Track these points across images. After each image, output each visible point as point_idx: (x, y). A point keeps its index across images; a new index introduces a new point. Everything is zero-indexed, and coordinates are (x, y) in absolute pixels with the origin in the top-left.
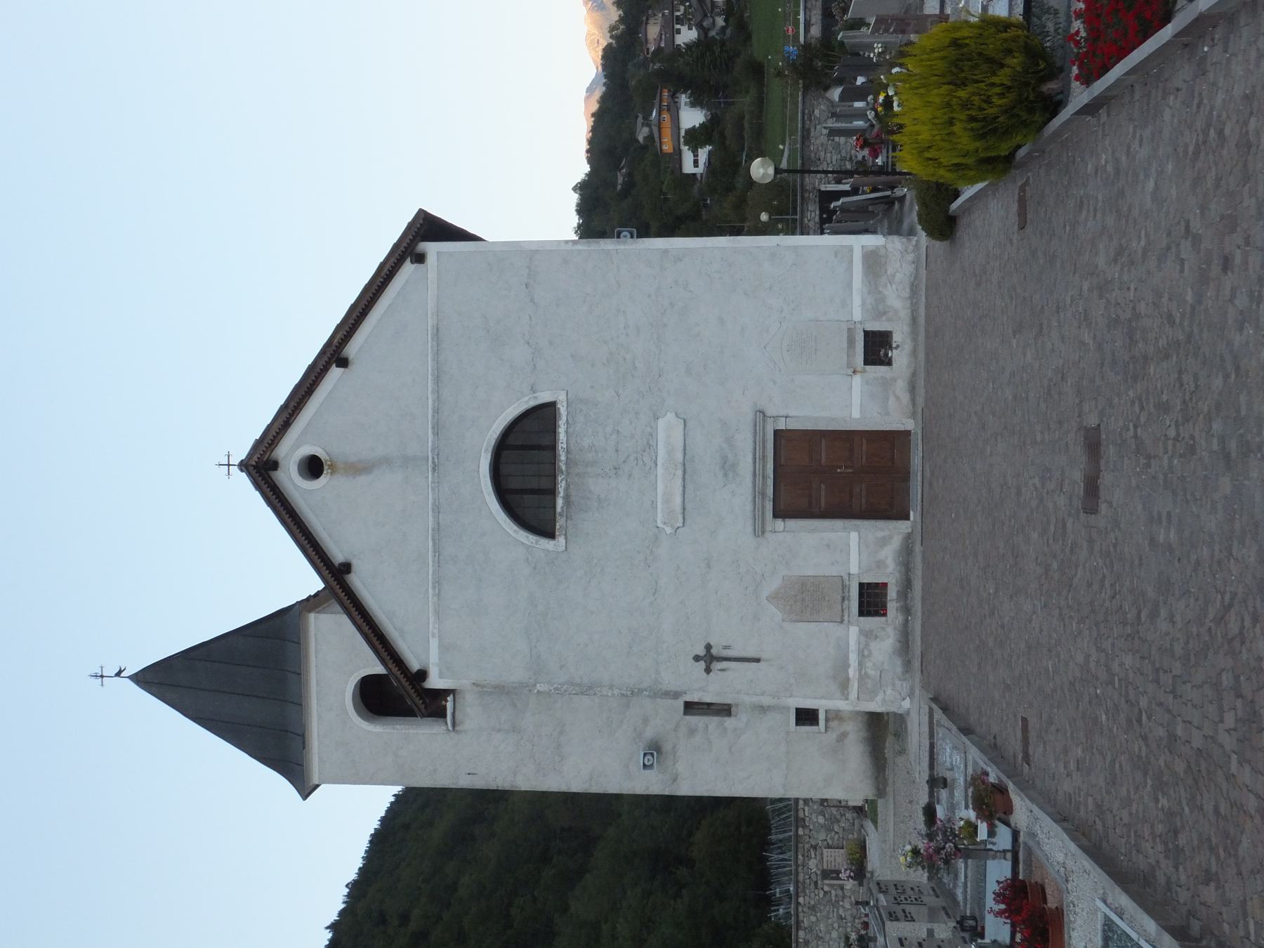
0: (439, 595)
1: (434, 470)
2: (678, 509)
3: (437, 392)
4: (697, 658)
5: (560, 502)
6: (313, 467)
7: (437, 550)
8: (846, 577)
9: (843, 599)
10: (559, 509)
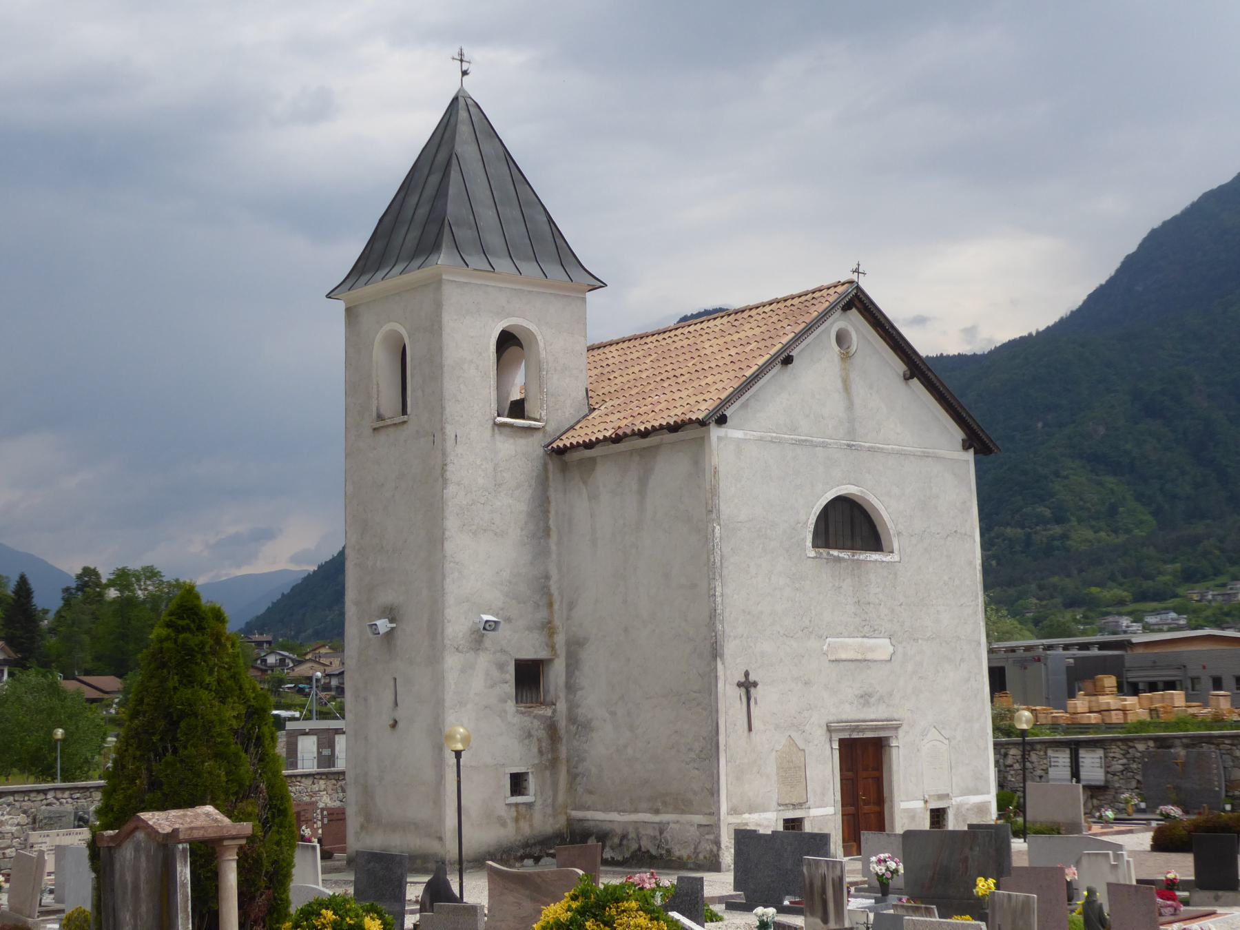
1: (848, 445)
4: (747, 674)
5: (835, 553)
6: (841, 339)
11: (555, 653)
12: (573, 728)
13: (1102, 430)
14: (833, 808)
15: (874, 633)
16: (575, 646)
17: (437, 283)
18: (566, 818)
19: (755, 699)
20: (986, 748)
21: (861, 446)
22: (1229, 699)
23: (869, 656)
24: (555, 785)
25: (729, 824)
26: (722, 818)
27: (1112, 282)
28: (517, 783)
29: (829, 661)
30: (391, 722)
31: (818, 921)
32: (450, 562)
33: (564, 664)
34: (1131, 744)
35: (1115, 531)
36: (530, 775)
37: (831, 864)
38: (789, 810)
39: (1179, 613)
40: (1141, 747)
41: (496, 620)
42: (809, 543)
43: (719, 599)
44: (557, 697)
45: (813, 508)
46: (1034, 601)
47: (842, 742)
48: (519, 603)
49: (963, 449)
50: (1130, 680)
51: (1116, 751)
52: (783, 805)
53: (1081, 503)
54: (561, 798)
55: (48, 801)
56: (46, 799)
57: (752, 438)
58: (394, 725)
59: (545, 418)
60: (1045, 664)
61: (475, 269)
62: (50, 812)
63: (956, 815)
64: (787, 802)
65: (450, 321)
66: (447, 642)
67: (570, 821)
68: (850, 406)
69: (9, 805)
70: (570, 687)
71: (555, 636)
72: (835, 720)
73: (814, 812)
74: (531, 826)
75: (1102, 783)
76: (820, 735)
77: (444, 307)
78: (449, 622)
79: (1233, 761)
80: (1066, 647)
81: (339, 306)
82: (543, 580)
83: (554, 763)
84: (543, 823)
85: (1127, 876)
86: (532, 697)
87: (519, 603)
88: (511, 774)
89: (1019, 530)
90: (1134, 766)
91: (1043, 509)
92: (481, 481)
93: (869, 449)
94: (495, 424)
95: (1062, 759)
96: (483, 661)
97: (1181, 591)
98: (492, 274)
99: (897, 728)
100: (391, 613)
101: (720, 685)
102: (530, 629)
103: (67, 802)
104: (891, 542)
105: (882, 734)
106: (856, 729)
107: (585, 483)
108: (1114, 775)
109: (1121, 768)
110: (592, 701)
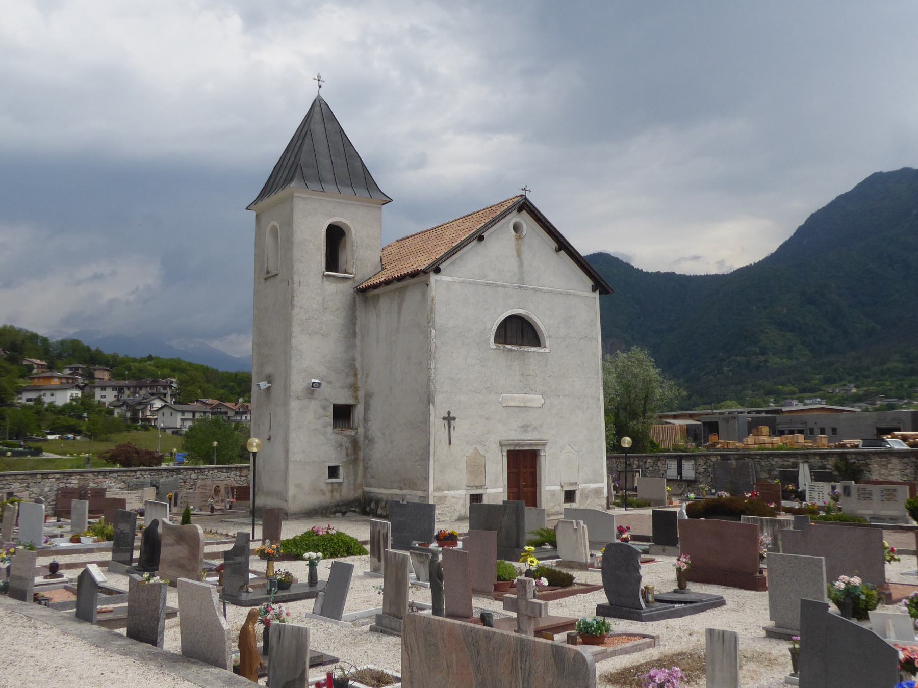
0: (470, 283)
1: (519, 287)
2: (509, 404)
3: (547, 292)
4: (449, 413)
5: (509, 347)
6: (516, 228)
7: (488, 285)
8: (485, 487)
9: (476, 486)
10: (506, 346)
11: (358, 401)
12: (366, 442)
13: (785, 311)
14: (502, 489)
15: (532, 391)
16: (368, 396)
17: (291, 198)
18: (362, 491)
19: (454, 427)
20: (602, 458)
21: (527, 287)
22: (827, 439)
23: (529, 404)
24: (356, 473)
25: (434, 496)
26: (430, 492)
27: (791, 239)
28: (333, 472)
29: (503, 406)
30: (268, 437)
31: (376, 560)
32: (295, 350)
33: (363, 408)
34: (709, 458)
35: (791, 359)
36: (341, 468)
37: (383, 524)
38: (473, 489)
39: (822, 399)
40: (714, 459)
41: (319, 382)
42: (492, 341)
43: (433, 371)
44: (358, 425)
45: (495, 321)
46: (750, 392)
47: (509, 452)
48: (336, 373)
49: (592, 291)
50: (779, 429)
51: (701, 461)
52: (470, 486)
53: (774, 346)
54: (359, 480)
55: (137, 476)
56: (136, 475)
57: (457, 281)
58: (269, 439)
59: (355, 273)
60: (738, 420)
61: (313, 190)
62: (137, 482)
63: (581, 495)
64: (473, 485)
65: (298, 217)
66: (292, 394)
67: (364, 493)
68: (521, 265)
69: (114, 478)
70: (366, 420)
71: (358, 392)
72: (505, 439)
73: (489, 491)
74: (341, 495)
75: (693, 479)
76: (495, 448)
77: (294, 211)
78: (293, 383)
79: (761, 468)
80: (749, 412)
81: (252, 214)
82: (351, 361)
83: (355, 461)
84: (348, 493)
85: (424, 548)
86: (345, 425)
87: (336, 373)
88: (329, 467)
89: (744, 358)
90: (710, 470)
91: (755, 348)
92: (315, 306)
93: (532, 289)
94: (324, 275)
95: (673, 465)
96: (314, 405)
97: (823, 388)
98: (324, 193)
99: (545, 445)
100: (269, 379)
101: (432, 418)
102: (343, 388)
103: (148, 477)
104: (545, 343)
105: (535, 448)
106: (517, 445)
107: (375, 308)
108: (700, 474)
109: (703, 470)
110: (375, 427)
